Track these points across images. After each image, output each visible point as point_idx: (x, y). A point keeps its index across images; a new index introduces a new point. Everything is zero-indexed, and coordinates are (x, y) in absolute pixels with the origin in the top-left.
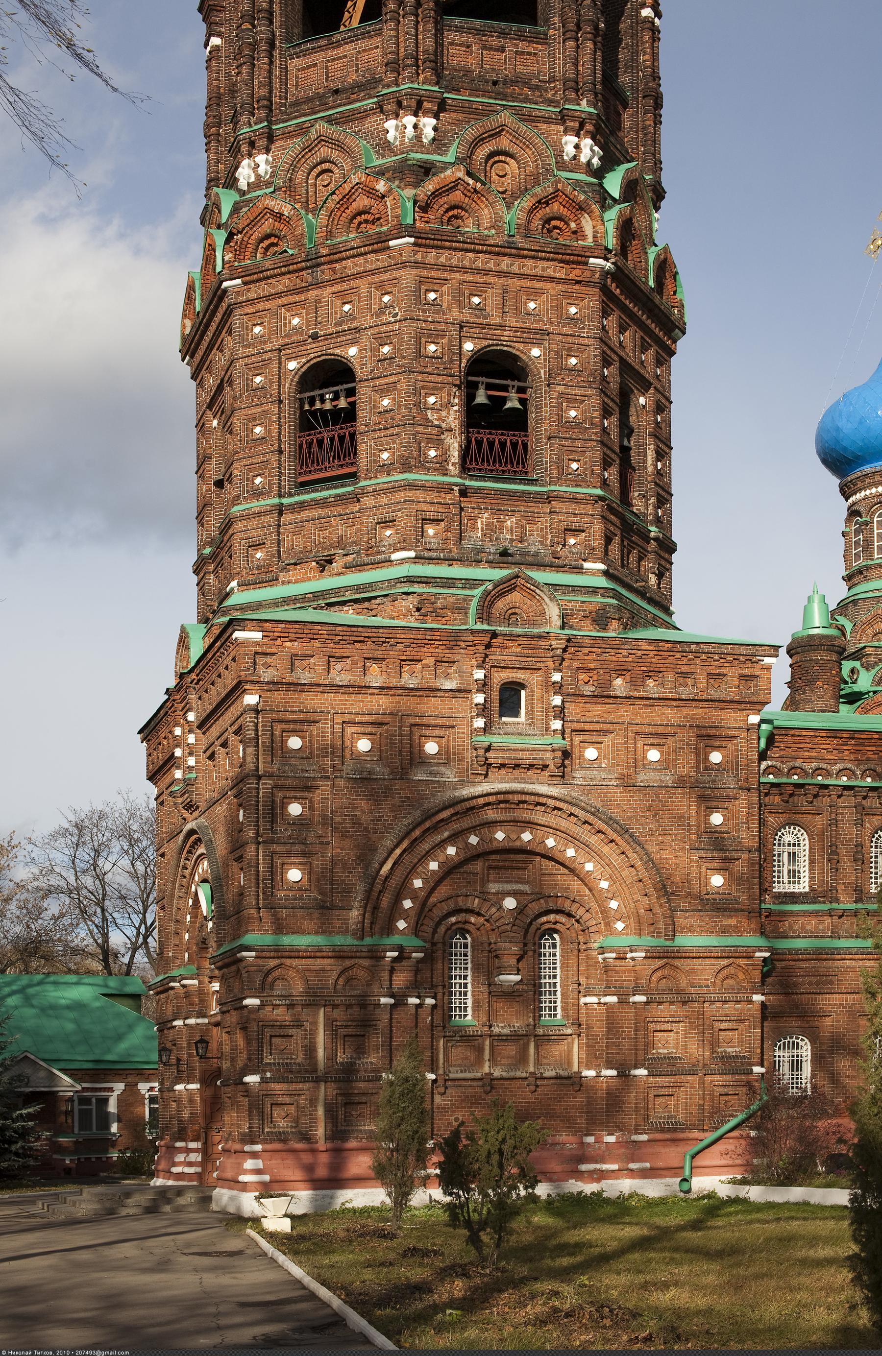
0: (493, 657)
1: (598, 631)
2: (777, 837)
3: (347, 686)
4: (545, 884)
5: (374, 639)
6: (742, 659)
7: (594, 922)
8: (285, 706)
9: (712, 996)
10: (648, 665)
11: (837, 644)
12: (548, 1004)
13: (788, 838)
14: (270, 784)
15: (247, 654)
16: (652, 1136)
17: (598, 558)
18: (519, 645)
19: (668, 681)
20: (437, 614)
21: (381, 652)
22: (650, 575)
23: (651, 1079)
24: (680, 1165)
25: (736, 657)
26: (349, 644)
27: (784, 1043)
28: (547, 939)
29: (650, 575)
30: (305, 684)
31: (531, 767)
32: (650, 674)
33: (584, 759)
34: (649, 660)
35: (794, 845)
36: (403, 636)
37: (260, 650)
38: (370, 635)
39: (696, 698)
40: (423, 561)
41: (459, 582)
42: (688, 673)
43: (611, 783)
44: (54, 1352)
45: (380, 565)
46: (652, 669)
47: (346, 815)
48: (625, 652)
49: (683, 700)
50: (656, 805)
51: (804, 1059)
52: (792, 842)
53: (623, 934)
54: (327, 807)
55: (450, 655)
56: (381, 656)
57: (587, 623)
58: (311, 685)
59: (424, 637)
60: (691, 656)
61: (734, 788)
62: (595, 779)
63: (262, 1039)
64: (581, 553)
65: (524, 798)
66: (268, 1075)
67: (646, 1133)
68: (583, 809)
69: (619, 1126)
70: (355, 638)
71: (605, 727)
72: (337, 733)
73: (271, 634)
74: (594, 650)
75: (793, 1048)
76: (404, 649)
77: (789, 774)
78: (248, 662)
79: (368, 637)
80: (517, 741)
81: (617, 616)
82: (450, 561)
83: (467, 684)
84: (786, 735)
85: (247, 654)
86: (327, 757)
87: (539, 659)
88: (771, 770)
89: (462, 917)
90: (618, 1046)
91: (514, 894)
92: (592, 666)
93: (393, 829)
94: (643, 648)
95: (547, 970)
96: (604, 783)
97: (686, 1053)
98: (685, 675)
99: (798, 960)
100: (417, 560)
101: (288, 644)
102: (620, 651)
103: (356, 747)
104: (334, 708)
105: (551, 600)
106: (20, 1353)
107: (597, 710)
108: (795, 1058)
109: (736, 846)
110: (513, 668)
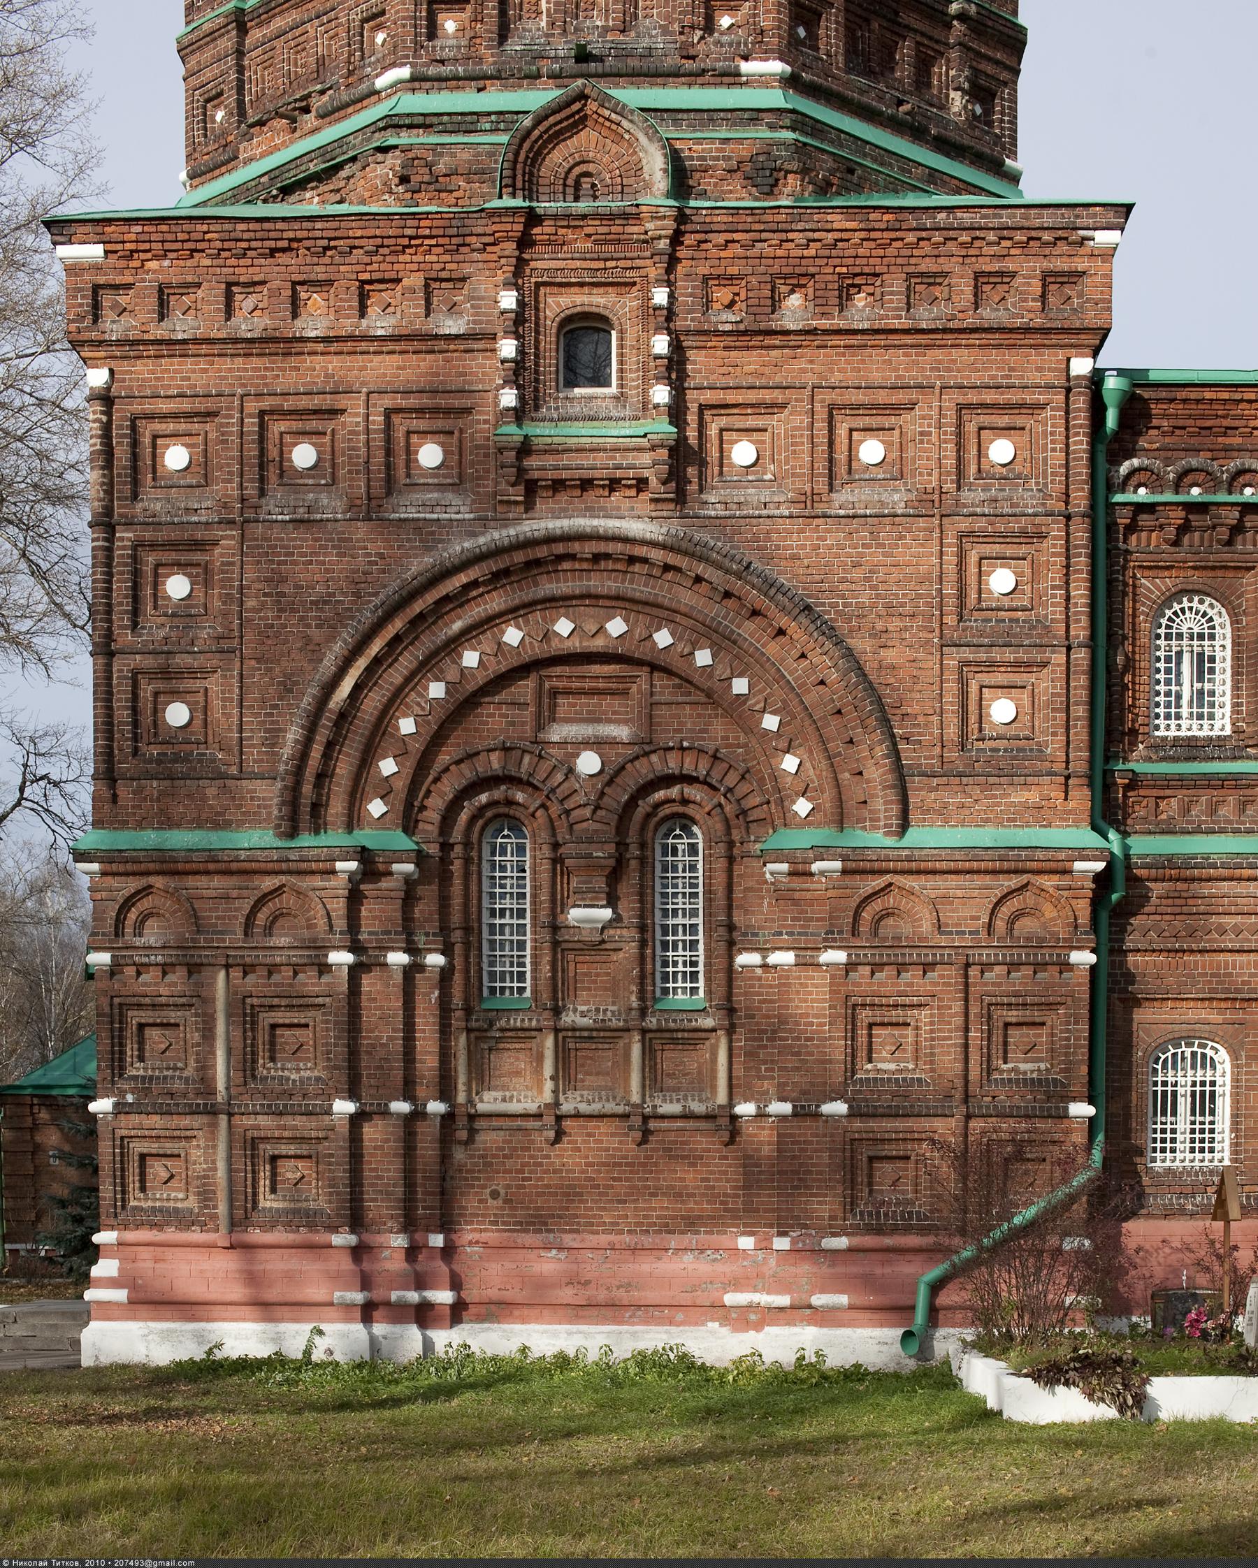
0: (539, 264)
1: (756, 199)
2: (1164, 621)
3: (261, 340)
4: (659, 724)
5: (307, 243)
6: (1047, 237)
7: (758, 800)
8: (156, 387)
9: (985, 952)
10: (850, 261)
12: (680, 968)
13: (1189, 624)
14: (129, 539)
15: (80, 290)
16: (858, 1241)
17: (772, 51)
18: (589, 236)
19: (892, 293)
20: (437, 184)
21: (323, 269)
22: (952, 94)
23: (858, 1124)
24: (909, 1303)
25: (1034, 234)
26: (262, 255)
27: (1174, 1055)
28: (680, 837)
29: (952, 94)
30: (184, 342)
31: (614, 485)
32: (857, 281)
33: (732, 465)
34: (852, 252)
35: (1201, 637)
36: (359, 233)
37: (101, 279)
38: (300, 234)
39: (951, 325)
40: (428, 85)
41: (485, 119)
42: (935, 275)
43: (777, 512)
44: (82, 1561)
45: (365, 103)
46: (858, 270)
47: (265, 595)
48: (799, 238)
49: (923, 331)
50: (871, 555)
52: (1196, 630)
53: (810, 824)
54: (231, 579)
55: (454, 266)
56: (322, 277)
57: (736, 183)
58: (197, 341)
59: (399, 232)
61: (1035, 515)
62: (746, 503)
63: (121, 1030)
64: (739, 43)
65: (602, 547)
66: (130, 1098)
67: (847, 1235)
68: (719, 567)
69: (798, 1218)
70: (272, 244)
71: (768, 396)
72: (249, 433)
73: (119, 247)
74: (736, 236)
75: (1194, 1067)
76: (367, 259)
77: (1177, 487)
78: (81, 305)
79: (300, 240)
80: (584, 432)
81: (795, 166)
82: (480, 80)
83: (488, 322)
84: (1172, 401)
85: (80, 290)
86: (230, 481)
87: (629, 263)
88: (1142, 477)
89: (499, 793)
90: (798, 1054)
91: (596, 744)
92: (733, 270)
93: (352, 618)
94: (836, 226)
95: (680, 899)
96: (764, 512)
97: (933, 1070)
98: (933, 279)
99: (1193, 880)
100: (417, 85)
101: (153, 265)
102: (790, 236)
103: (290, 461)
104: (244, 385)
105: (650, 139)
106: (30, 1564)
107: (751, 362)
108: (1169, 1089)
109: (1040, 636)
110: (582, 285)
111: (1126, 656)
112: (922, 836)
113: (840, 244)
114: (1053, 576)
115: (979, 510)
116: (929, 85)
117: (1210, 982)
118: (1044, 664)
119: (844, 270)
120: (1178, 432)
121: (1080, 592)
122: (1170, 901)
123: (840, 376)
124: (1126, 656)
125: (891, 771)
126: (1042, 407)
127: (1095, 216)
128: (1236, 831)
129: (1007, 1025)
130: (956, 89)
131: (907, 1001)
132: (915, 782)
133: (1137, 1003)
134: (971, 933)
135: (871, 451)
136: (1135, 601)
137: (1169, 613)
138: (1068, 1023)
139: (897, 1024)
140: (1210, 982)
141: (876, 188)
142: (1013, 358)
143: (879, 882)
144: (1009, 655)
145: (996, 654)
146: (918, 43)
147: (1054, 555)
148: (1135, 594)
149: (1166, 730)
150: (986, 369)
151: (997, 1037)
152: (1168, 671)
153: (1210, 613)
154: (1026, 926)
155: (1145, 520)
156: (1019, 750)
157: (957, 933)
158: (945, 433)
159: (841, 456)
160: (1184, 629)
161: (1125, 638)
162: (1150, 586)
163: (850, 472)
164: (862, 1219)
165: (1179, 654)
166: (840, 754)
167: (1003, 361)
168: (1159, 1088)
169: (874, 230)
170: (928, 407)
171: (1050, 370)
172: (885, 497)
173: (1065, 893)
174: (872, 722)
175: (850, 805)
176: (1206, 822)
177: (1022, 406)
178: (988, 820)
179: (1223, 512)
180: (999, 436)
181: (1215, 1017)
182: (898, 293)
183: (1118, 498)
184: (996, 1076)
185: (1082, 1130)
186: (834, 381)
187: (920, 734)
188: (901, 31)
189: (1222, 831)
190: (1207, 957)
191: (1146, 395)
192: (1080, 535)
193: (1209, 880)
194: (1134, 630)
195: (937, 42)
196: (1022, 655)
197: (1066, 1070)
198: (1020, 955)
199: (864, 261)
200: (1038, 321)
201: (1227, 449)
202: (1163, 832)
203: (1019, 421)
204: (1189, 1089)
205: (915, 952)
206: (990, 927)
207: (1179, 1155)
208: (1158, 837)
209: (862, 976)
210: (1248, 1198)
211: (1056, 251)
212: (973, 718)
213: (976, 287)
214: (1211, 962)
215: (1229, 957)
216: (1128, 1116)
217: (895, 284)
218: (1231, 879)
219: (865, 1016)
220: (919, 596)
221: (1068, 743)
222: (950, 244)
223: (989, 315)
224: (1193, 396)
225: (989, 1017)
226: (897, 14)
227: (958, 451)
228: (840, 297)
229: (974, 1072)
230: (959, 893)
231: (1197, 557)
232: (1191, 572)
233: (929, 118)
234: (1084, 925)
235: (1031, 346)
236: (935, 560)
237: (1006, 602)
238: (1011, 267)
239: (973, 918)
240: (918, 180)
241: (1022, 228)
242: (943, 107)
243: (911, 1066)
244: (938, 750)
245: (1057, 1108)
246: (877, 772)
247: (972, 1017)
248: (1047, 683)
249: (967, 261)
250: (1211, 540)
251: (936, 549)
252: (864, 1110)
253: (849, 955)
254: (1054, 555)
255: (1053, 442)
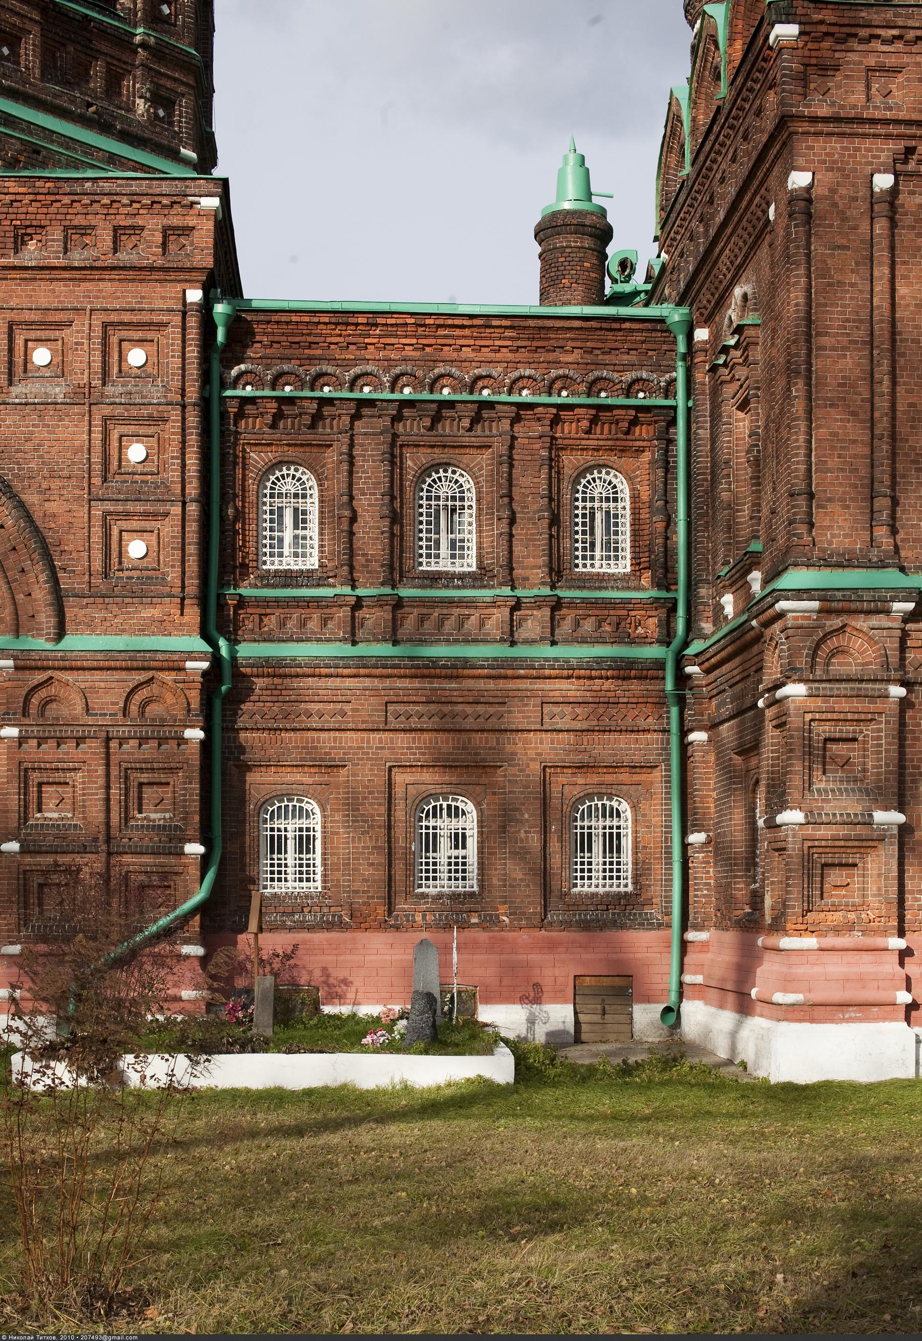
6: (165, 201)
10: (23, 216)
11: (588, 222)
13: (289, 486)
19: (53, 240)
22: (138, 101)
23: (28, 859)
25: (156, 199)
29: (138, 101)
32: (29, 231)
34: (24, 210)
39: (96, 264)
42: (85, 227)
46: (28, 223)
49: (75, 269)
51: (468, 833)
52: (293, 491)
60: (86, 201)
61: (159, 404)
67: (21, 943)
84: (269, 322)
88: (249, 378)
94: (11, 190)
99: (285, 676)
108: (586, 831)
109: (163, 494)
111: (236, 509)
112: (74, 642)
113: (15, 204)
114: (173, 450)
115: (117, 400)
116: (120, 94)
117: (301, 753)
118: (166, 514)
119: (18, 223)
120: (275, 345)
121: (193, 461)
122: (269, 692)
123: (16, 300)
124: (236, 509)
125: (51, 593)
126: (166, 325)
127: (200, 186)
128: (319, 640)
129: (141, 785)
130: (140, 97)
131: (65, 766)
132: (70, 604)
133: (249, 768)
134: (111, 715)
135: (41, 356)
136: (244, 469)
137: (583, 481)
138: (185, 783)
139: (60, 783)
140: (301, 753)
141: (58, 164)
142: (144, 289)
143: (41, 677)
144: (140, 508)
145: (130, 507)
146: (108, 63)
147: (173, 434)
148: (244, 464)
149: (272, 565)
150: (124, 297)
151: (133, 793)
152: (584, 524)
153: (615, 481)
154: (154, 710)
155: (249, 409)
156: (148, 578)
157: (101, 715)
158: (94, 343)
159: (19, 359)
160: (596, 495)
161: (235, 496)
162: (257, 458)
163: (25, 371)
164: (33, 931)
165: (437, 512)
166: (16, 580)
167: (137, 292)
168: (424, 831)
169: (39, 194)
170: (81, 324)
171: (171, 298)
172: (49, 390)
173: (181, 685)
174: (36, 556)
175: (23, 618)
176: (296, 633)
177: (150, 324)
178: (124, 631)
179: (306, 404)
180: (135, 346)
181: (307, 779)
182: (57, 240)
183: (229, 393)
184: (132, 823)
185: (196, 864)
186: (12, 304)
187: (73, 566)
188: (95, 54)
189: (308, 640)
190: (298, 734)
191: (249, 318)
192: (193, 419)
193: (297, 676)
194: (244, 490)
195: (125, 63)
196: (149, 508)
197: (184, 819)
198: (147, 732)
199: (33, 217)
200: (160, 262)
201: (311, 358)
202: (265, 641)
203: (149, 335)
204: (601, 831)
205: (70, 728)
206: (125, 711)
207: (594, 881)
208: (262, 644)
209: (31, 747)
210: (333, 916)
211: (173, 212)
212: (115, 554)
213: (115, 237)
214: (302, 738)
215: (315, 735)
216: (243, 854)
217: (57, 234)
218: (314, 676)
219: (35, 777)
220: (74, 463)
221: (183, 573)
222: (95, 205)
223: (125, 257)
224: (283, 319)
225: (127, 777)
226: (91, 41)
227: (104, 357)
228: (15, 242)
229: (115, 819)
230: (102, 685)
231: (289, 437)
232: (286, 448)
233: (116, 117)
234: (196, 710)
235: (156, 281)
236: (86, 437)
237: (140, 469)
238: (141, 223)
239: (113, 704)
240: (99, 161)
241: (147, 195)
242: (131, 108)
243: (70, 815)
244: (87, 577)
245: (176, 847)
246: (41, 594)
247: (112, 779)
248: (169, 529)
249: (108, 218)
250: (300, 425)
251: (86, 429)
252: (32, 848)
253: (21, 731)
254: (173, 434)
255: (173, 351)
